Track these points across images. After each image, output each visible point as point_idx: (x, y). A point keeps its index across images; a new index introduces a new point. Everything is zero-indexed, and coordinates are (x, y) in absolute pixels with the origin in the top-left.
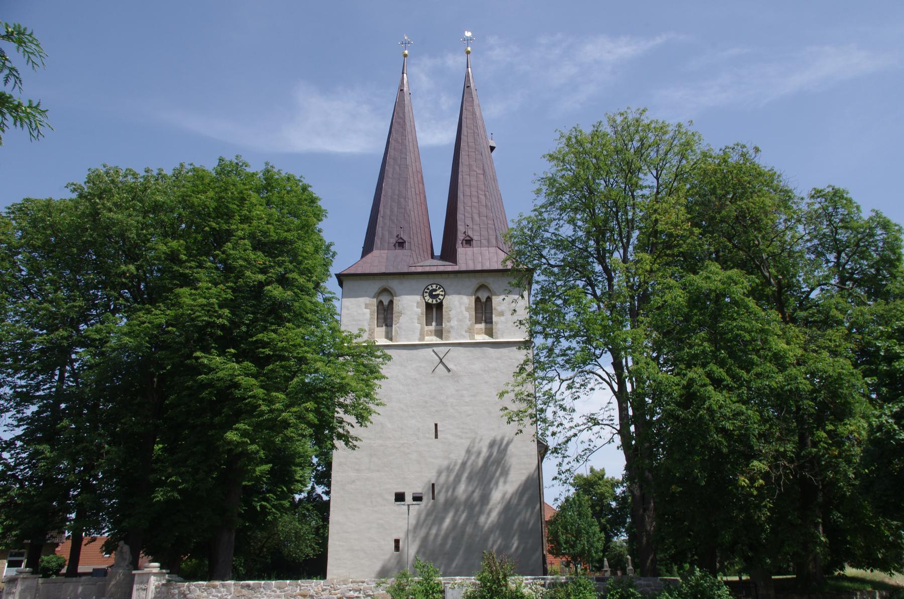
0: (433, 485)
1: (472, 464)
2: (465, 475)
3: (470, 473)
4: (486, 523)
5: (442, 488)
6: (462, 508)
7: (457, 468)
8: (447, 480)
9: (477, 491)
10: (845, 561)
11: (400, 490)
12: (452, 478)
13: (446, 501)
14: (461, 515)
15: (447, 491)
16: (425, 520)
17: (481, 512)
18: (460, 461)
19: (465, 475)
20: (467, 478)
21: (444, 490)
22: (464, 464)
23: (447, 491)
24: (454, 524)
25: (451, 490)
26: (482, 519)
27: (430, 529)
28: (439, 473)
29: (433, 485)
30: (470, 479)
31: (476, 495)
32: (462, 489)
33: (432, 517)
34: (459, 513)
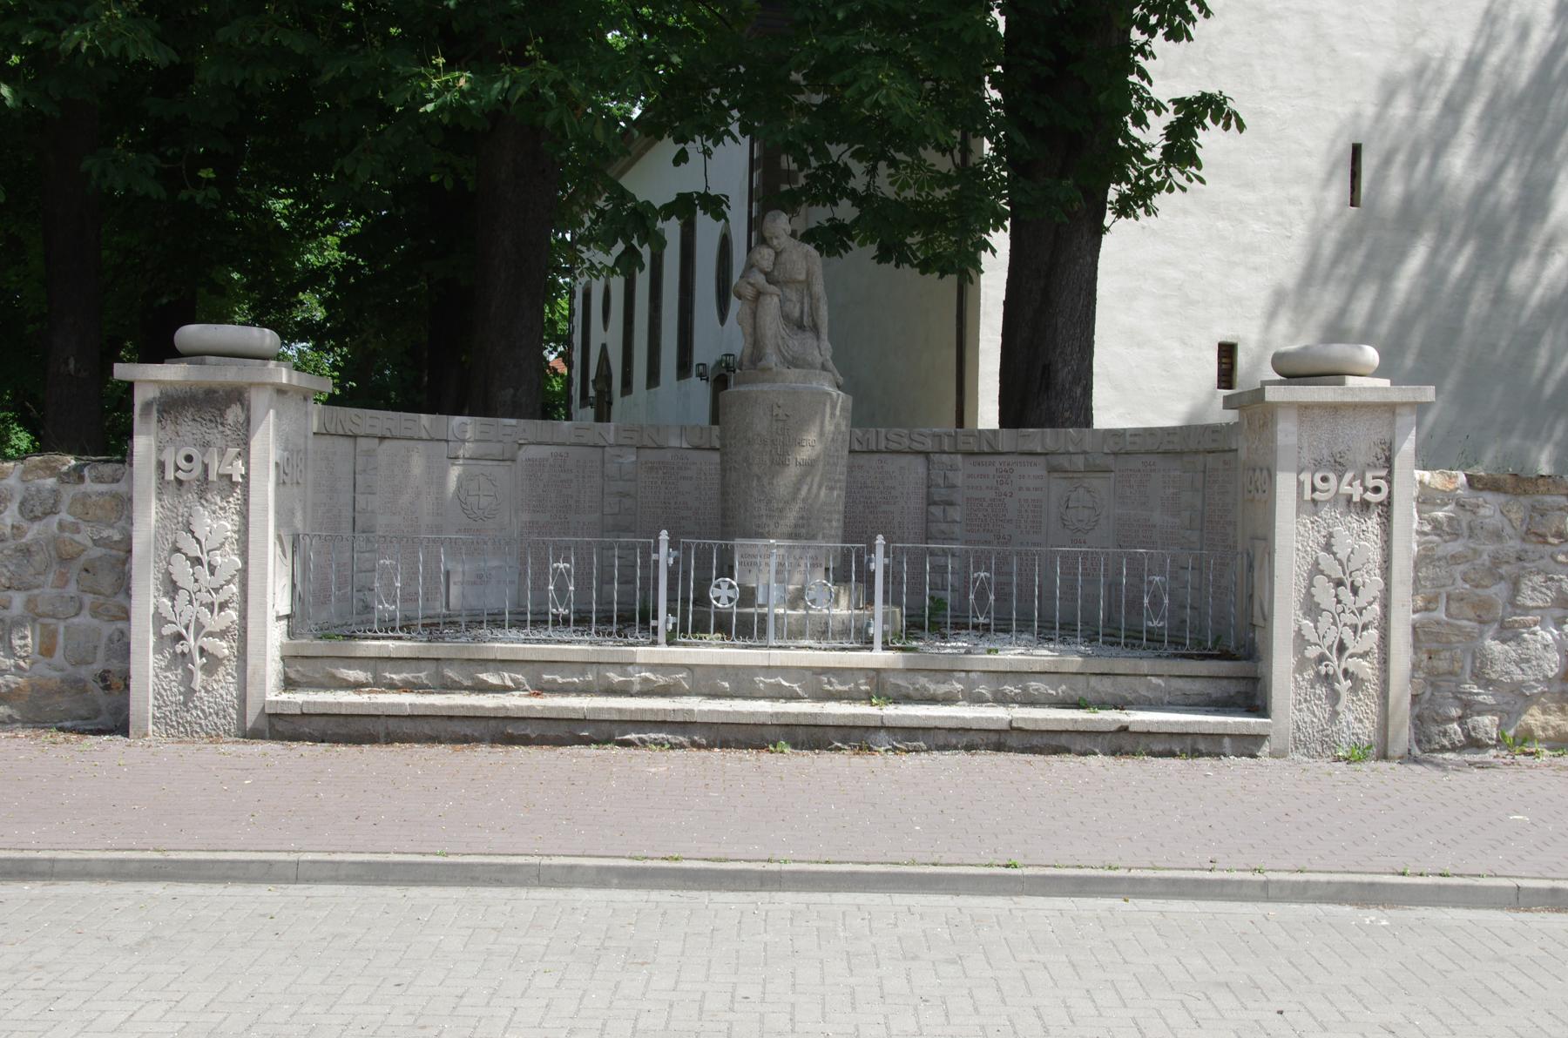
0: (1356, 150)
1: (1499, 72)
2: (1475, 110)
3: (1492, 104)
4: (1530, 289)
5: (1387, 161)
6: (1457, 230)
7: (1454, 69)
8: (1411, 121)
9: (1510, 173)
10: (1241, 416)
11: (1228, 338)
12: (1433, 109)
13: (1408, 200)
14: (1452, 257)
15: (1412, 163)
16: (1336, 261)
17: (1518, 251)
18: (1460, 55)
19: (1475, 110)
20: (1481, 119)
21: (1401, 158)
22: (1472, 67)
23: (1412, 163)
24: (1434, 272)
25: (1424, 162)
26: (1520, 276)
27: (1351, 296)
28: (1387, 99)
29: (1356, 150)
30: (1490, 118)
31: (1508, 189)
32: (1461, 165)
33: (1359, 257)
34: (1451, 244)
